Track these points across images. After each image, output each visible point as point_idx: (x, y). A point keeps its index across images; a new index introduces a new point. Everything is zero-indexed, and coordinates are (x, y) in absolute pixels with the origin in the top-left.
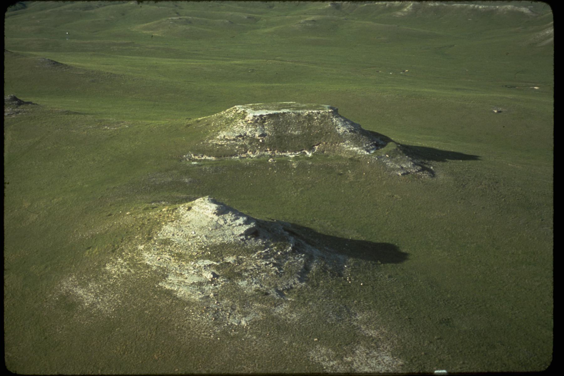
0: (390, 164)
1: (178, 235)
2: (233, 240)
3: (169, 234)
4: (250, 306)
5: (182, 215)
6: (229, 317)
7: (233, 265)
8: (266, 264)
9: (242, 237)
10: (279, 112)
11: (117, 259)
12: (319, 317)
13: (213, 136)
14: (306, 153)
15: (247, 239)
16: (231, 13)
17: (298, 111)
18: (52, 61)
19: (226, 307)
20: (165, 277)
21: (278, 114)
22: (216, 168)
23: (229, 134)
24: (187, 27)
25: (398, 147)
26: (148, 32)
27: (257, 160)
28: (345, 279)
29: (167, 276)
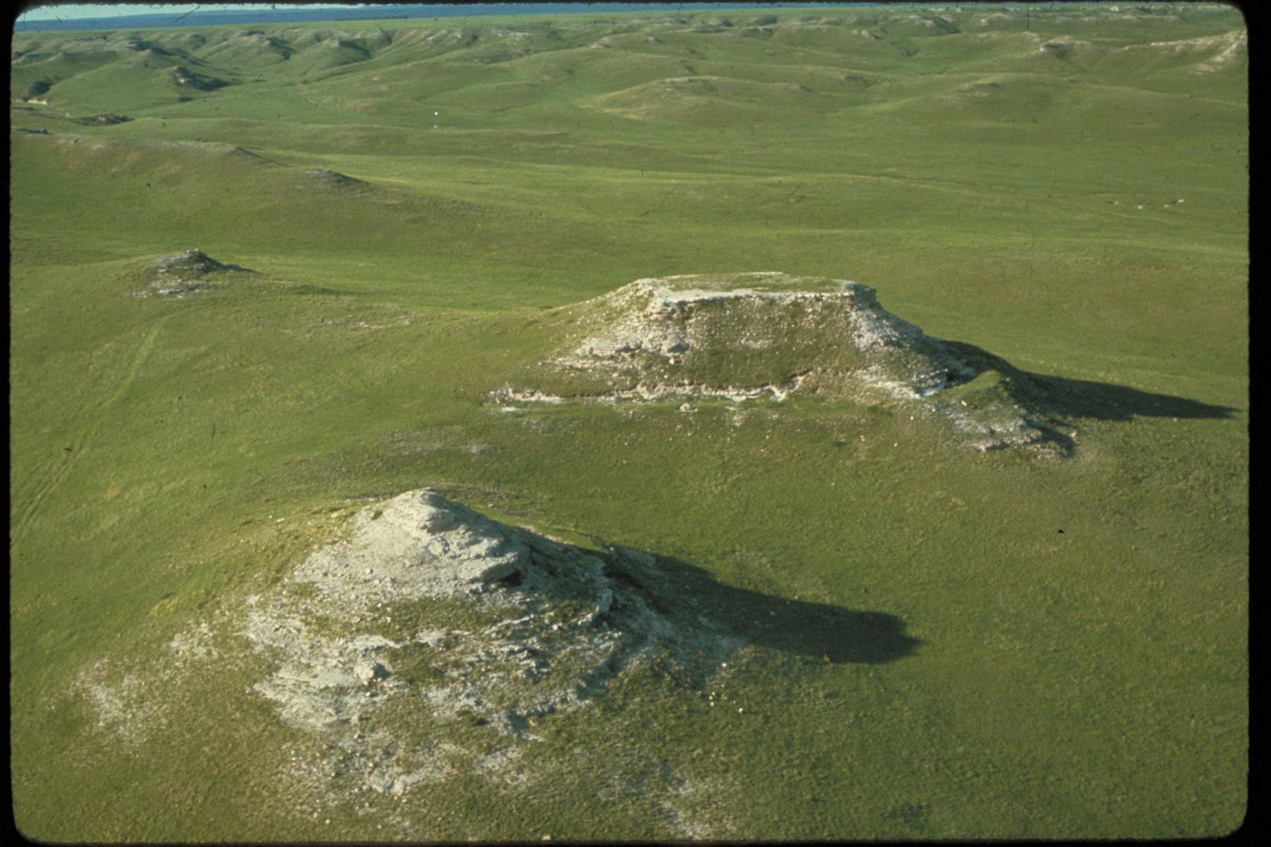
0: (963, 423)
1: (335, 575)
2: (451, 591)
3: (317, 571)
5: (359, 529)
6: (370, 773)
7: (432, 650)
8: (512, 652)
9: (474, 587)
10: (725, 294)
12: (582, 786)
14: (773, 393)
17: (771, 294)
18: (336, 175)
19: (375, 748)
20: (272, 669)
23: (602, 345)
24: (703, 100)
26: (616, 111)
27: (659, 405)
29: (278, 669)
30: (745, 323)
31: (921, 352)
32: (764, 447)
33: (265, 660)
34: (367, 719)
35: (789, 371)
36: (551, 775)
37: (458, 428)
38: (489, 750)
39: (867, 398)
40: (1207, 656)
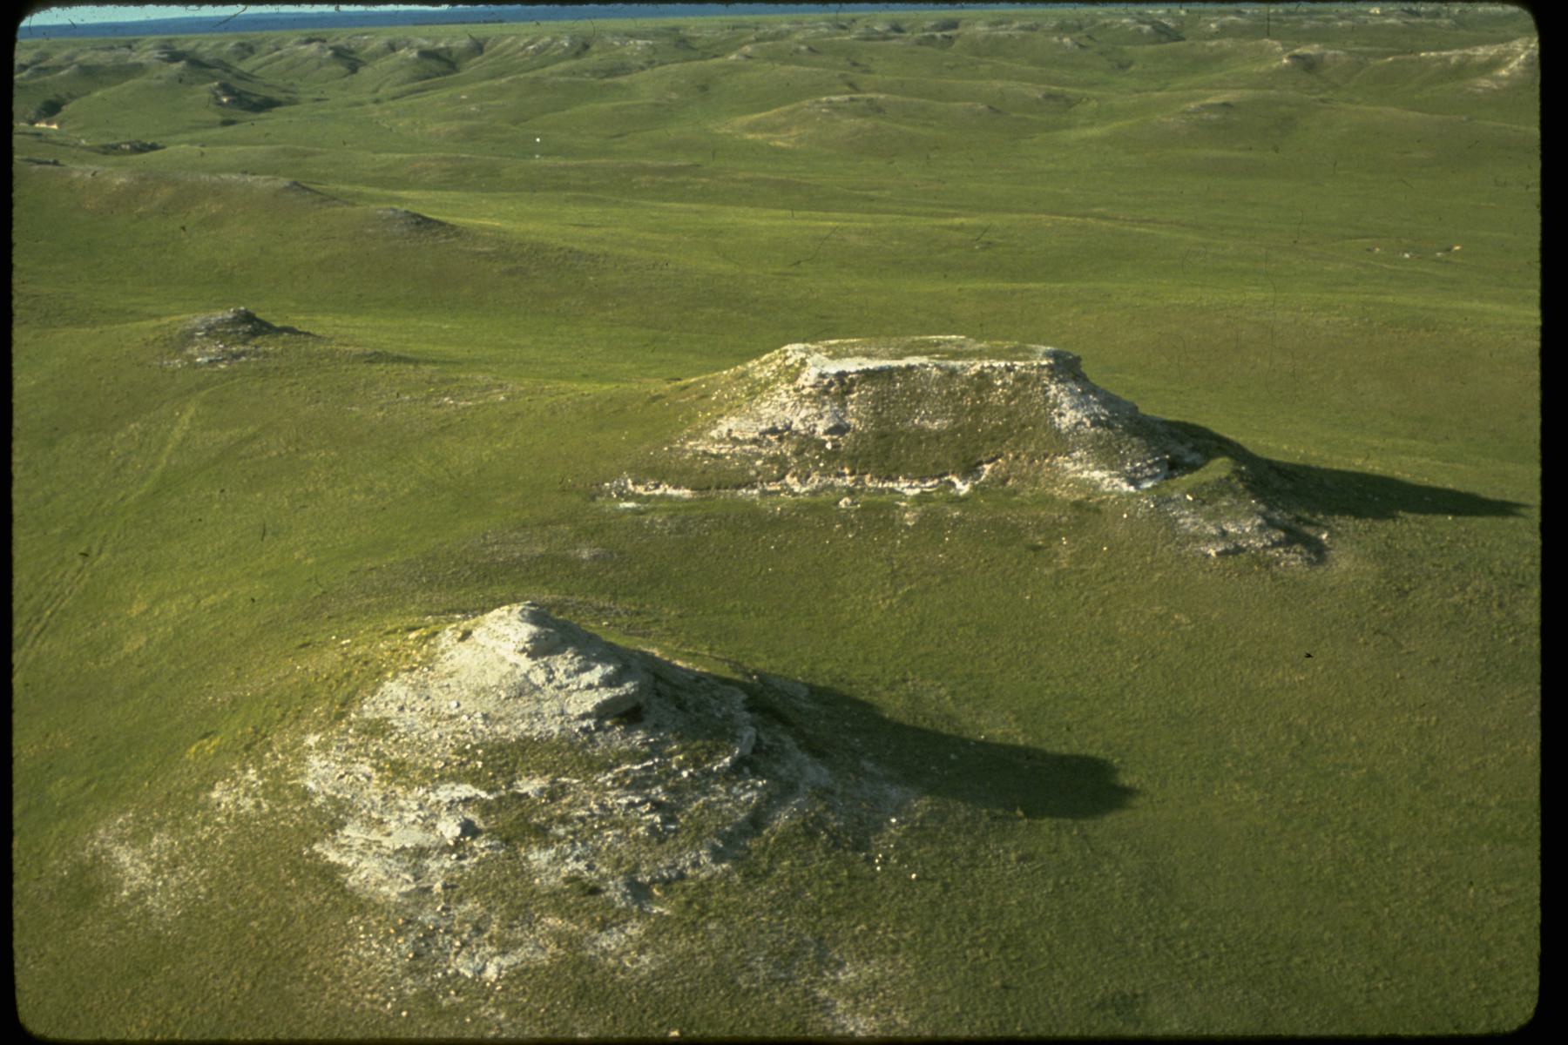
0: (1188, 521)
1: (413, 710)
2: (556, 730)
3: (391, 705)
4: (530, 924)
5: (443, 653)
7: (533, 802)
8: (631, 805)
10: (895, 363)
12: (718, 970)
13: (703, 428)
14: (953, 485)
15: (599, 728)
16: (998, 84)
17: (952, 363)
18: (415, 216)
19: (462, 923)
21: (891, 370)
24: (868, 124)
25: (1237, 472)
26: (760, 137)
27: (812, 500)
28: (869, 860)
29: (342, 825)
30: (919, 399)
31: (1136, 435)
32: (943, 551)
33: (327, 814)
34: (453, 887)
38: (604, 926)
39: (1071, 491)
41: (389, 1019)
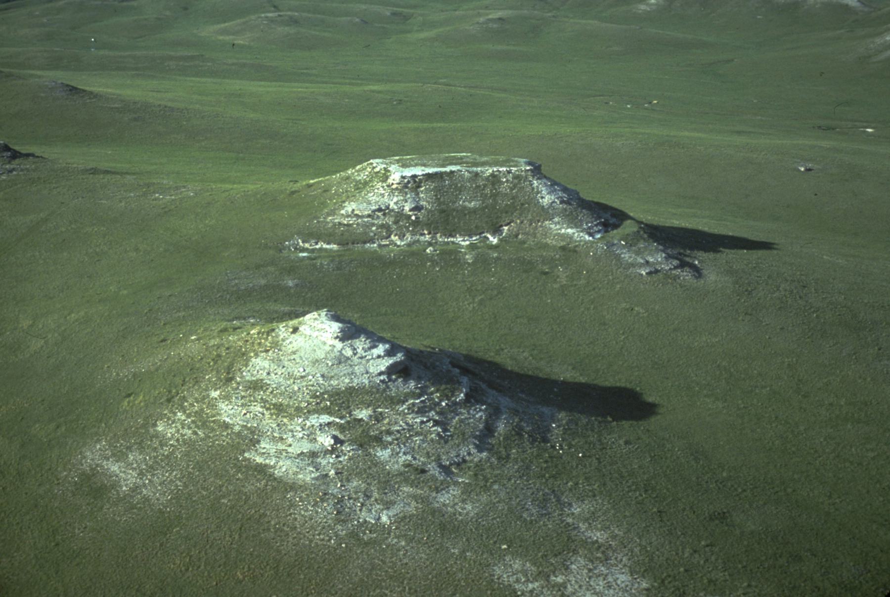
0: (627, 256)
1: (276, 374)
2: (367, 382)
3: (261, 372)
4: (396, 492)
5: (283, 340)
6: (361, 510)
7: (367, 424)
8: (422, 422)
9: (382, 378)
10: (443, 170)
11: (175, 414)
12: (511, 510)
13: (335, 209)
14: (488, 239)
15: (390, 380)
17: (475, 169)
18: (68, 85)
19: (356, 493)
20: (254, 443)
22: (340, 262)
23: (361, 207)
26: (227, 38)
27: (407, 249)
28: (553, 447)
29: (258, 442)
30: (460, 190)
31: (583, 208)
32: (493, 276)
33: (246, 436)
34: (341, 473)
35: (497, 223)
36: (487, 505)
37: (271, 269)
39: (557, 240)
40: (842, 406)
41: (335, 550)
